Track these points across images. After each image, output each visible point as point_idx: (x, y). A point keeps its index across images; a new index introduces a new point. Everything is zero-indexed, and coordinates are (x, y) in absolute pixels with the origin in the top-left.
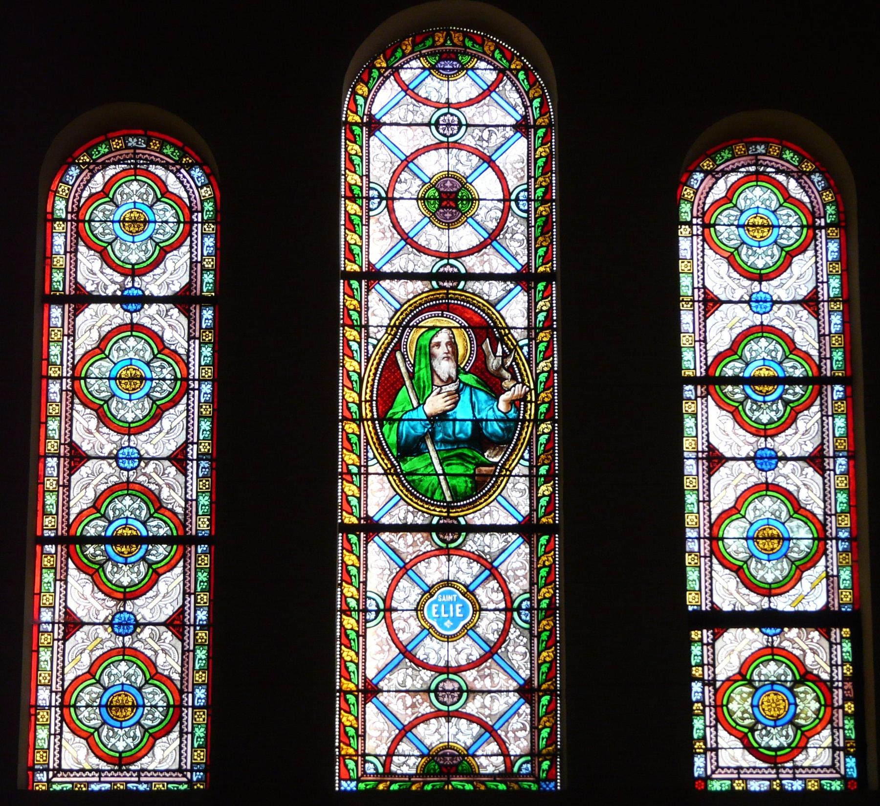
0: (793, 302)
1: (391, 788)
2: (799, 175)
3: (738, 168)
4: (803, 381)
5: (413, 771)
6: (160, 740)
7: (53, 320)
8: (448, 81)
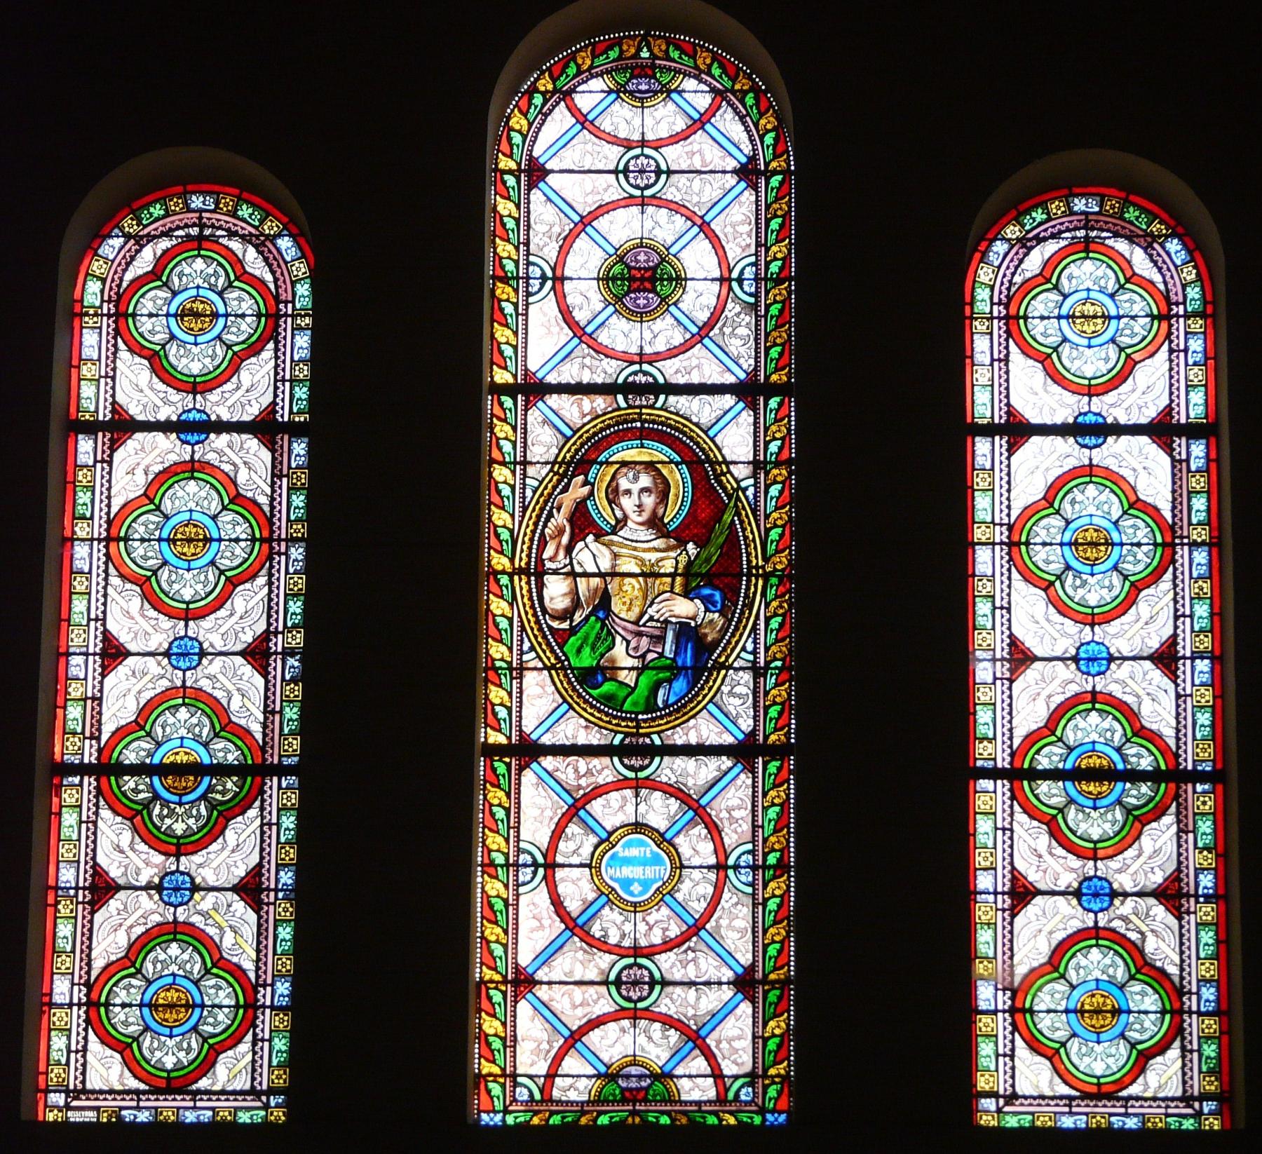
0: (1140, 894)
1: (551, 1122)
2: (1148, 242)
3: (1061, 232)
4: (1154, 776)
5: (585, 1098)
6: (224, 1055)
7: (54, 1054)
8: (643, 107)
